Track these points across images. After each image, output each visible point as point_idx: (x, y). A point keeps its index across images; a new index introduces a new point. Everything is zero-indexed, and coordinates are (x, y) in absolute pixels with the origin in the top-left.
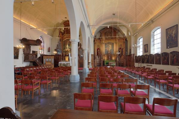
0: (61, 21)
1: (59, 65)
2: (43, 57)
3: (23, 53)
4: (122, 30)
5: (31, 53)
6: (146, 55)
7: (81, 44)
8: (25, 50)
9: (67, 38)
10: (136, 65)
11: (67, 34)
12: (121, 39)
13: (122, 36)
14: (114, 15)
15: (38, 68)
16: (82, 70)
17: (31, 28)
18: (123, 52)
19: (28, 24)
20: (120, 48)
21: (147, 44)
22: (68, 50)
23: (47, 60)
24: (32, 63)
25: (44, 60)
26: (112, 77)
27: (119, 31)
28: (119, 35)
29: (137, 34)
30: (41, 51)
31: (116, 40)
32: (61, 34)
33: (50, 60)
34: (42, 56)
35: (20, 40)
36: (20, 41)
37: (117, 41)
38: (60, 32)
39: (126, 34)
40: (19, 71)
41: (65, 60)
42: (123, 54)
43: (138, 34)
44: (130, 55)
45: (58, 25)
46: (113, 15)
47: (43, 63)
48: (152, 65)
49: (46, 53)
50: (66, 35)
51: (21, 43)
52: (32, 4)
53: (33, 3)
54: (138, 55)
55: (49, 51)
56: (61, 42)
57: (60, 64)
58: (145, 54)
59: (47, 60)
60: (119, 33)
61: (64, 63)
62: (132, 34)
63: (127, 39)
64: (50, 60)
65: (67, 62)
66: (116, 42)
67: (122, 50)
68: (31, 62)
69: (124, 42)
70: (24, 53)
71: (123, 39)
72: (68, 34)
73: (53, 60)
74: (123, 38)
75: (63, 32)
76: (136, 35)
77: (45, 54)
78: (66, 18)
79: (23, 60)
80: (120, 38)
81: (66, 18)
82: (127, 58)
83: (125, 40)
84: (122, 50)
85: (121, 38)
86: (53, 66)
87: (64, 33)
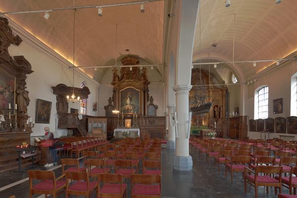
0: (116, 56)
1: (114, 135)
2: (87, 120)
3: (56, 112)
4: (219, 73)
5: (69, 112)
6: (279, 118)
7: (151, 97)
8: (60, 108)
9: (130, 86)
10: (253, 135)
11: (128, 79)
12: (218, 90)
13: (218, 85)
14: (215, 46)
15: (80, 142)
16: (166, 143)
17: (70, 67)
18: (221, 113)
19: (66, 58)
20: (217, 106)
21: (281, 99)
22: (130, 108)
23: (95, 125)
24: (72, 131)
25: (90, 125)
26: (29, 126)
27: (214, 77)
28: (214, 83)
29: (255, 81)
30: (82, 108)
31: (209, 91)
32: (117, 79)
33: (100, 125)
34: (86, 118)
35: (53, 88)
36: (53, 90)
37: (211, 93)
38: (115, 76)
39: (226, 82)
40: (61, 147)
41: (124, 126)
42: (221, 116)
43: (257, 81)
44: (238, 119)
45: (112, 62)
46: (213, 47)
47: (87, 129)
48: (294, 137)
49: (90, 113)
50: (127, 80)
51: (54, 93)
52: (99, 13)
53: (100, 11)
54: (256, 118)
55: (95, 110)
56: (150, 96)
57: (117, 133)
58: (275, 116)
59: (95, 125)
60: (214, 80)
61: (123, 130)
62: (243, 81)
63: (229, 91)
64: (100, 125)
65: (129, 130)
66: (209, 94)
67: (220, 109)
68: (69, 129)
69: (223, 96)
70: (58, 113)
71: (222, 91)
72: (129, 80)
73: (105, 125)
74: (220, 87)
75: (120, 75)
76: (252, 82)
77: (89, 115)
78: (127, 50)
79: (57, 125)
80: (216, 88)
81: (127, 50)
82: (228, 123)
83: (224, 92)
84: (220, 109)
85: (218, 88)
86: (105, 136)
87: (122, 78)
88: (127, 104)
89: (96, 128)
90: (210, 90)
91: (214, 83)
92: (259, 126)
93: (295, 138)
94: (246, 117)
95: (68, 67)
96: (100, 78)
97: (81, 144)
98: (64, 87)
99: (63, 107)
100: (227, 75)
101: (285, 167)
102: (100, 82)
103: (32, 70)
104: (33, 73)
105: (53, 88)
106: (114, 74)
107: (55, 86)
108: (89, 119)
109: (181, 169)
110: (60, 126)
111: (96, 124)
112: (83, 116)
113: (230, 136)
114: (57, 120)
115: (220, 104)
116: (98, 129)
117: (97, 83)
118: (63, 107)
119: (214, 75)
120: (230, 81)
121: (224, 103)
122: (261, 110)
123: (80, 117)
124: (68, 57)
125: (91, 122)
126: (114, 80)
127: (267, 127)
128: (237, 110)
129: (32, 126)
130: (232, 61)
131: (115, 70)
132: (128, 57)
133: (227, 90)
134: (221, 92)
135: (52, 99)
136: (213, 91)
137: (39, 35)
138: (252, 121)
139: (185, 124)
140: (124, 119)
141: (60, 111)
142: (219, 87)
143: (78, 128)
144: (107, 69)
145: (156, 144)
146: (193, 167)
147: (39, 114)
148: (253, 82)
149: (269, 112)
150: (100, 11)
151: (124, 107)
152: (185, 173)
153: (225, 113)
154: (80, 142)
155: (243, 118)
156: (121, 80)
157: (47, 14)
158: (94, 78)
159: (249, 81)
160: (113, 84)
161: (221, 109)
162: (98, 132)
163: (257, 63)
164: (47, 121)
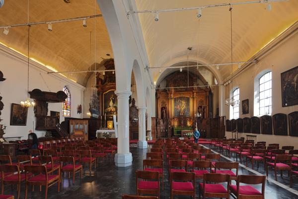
2: (69, 121)
4: (202, 75)
5: (49, 114)
6: (246, 119)
7: (133, 99)
10: (229, 135)
11: (111, 82)
13: (202, 86)
16: (136, 143)
17: (48, 73)
18: (205, 114)
21: (248, 100)
22: (112, 110)
25: (71, 127)
28: (198, 85)
30: (63, 110)
31: (193, 93)
32: (100, 82)
33: (81, 127)
34: (68, 120)
35: (29, 93)
37: (195, 94)
38: (98, 79)
39: (210, 83)
41: (107, 127)
42: (205, 117)
48: (256, 136)
50: (110, 84)
51: (31, 98)
53: (50, 27)
54: (231, 118)
57: (99, 134)
58: (243, 117)
60: (199, 82)
62: (221, 82)
63: (212, 92)
64: (81, 127)
66: (193, 96)
71: (206, 92)
73: (86, 127)
75: (103, 78)
76: (227, 83)
78: (108, 55)
80: (200, 89)
81: (108, 55)
83: (208, 93)
84: (204, 109)
85: (202, 89)
88: (110, 107)
91: (198, 85)
92: (234, 125)
93: (257, 137)
94: (223, 117)
95: (47, 73)
97: (49, 145)
99: (42, 110)
102: (85, 85)
103: (4, 77)
107: (31, 91)
109: (119, 165)
110: (38, 128)
111: (78, 125)
114: (35, 122)
117: (82, 87)
118: (42, 110)
119: (199, 77)
121: (207, 104)
125: (72, 124)
126: (97, 83)
131: (98, 74)
133: (210, 91)
135: (30, 103)
136: (197, 93)
138: (228, 121)
141: (38, 114)
142: (202, 88)
144: (92, 73)
145: (229, 153)
147: (13, 117)
148: (229, 84)
151: (107, 109)
152: (123, 169)
153: (209, 114)
158: (77, 83)
159: (226, 82)
160: (97, 87)
164: (23, 122)
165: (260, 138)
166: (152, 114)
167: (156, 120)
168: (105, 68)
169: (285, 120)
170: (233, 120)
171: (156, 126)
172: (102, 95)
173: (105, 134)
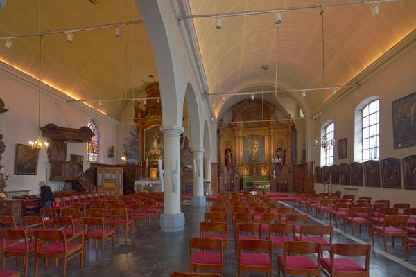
1: (135, 189)
2: (96, 169)
3: (47, 159)
5: (68, 159)
6: (343, 165)
7: (186, 138)
10: (319, 188)
13: (282, 120)
14: (266, 69)
16: (190, 199)
17: (68, 101)
18: (286, 158)
20: (280, 149)
21: (346, 139)
24: (71, 184)
25: (100, 176)
28: (276, 118)
31: (270, 129)
32: (140, 115)
33: (113, 176)
34: (95, 167)
35: (41, 129)
37: (272, 130)
38: (137, 110)
39: (292, 116)
42: (286, 163)
44: (304, 165)
48: (357, 190)
50: (153, 116)
53: (70, 37)
57: (138, 186)
59: (108, 176)
60: (278, 113)
63: (296, 127)
64: (113, 176)
65: (153, 182)
66: (270, 133)
67: (284, 152)
70: (50, 161)
71: (288, 128)
73: (120, 177)
75: (144, 109)
76: (317, 116)
77: (103, 163)
78: (151, 76)
79: (48, 177)
80: (279, 124)
81: (151, 76)
83: (290, 129)
84: (284, 152)
85: (283, 125)
89: (109, 180)
90: (270, 127)
94: (312, 163)
96: (118, 114)
98: (54, 128)
99: (58, 153)
100: (293, 106)
101: (265, 225)
104: (8, 112)
105: (41, 129)
106: (135, 108)
107: (44, 126)
108: (99, 169)
111: (108, 175)
112: (92, 164)
113: (295, 189)
115: (285, 146)
116: (111, 183)
120: (298, 115)
122: (327, 158)
123: (86, 167)
124: (64, 90)
125: (101, 172)
126: (136, 116)
127: (333, 178)
128: (304, 158)
129: (5, 178)
130: (274, 93)
131: (138, 103)
132: (153, 85)
133: (293, 128)
134: (286, 130)
137: (17, 65)
138: (318, 168)
139: (172, 175)
140: (149, 168)
143: (82, 180)
146: (185, 225)
149: (334, 156)
150: (70, 37)
152: (172, 234)
154: (83, 197)
155: (309, 165)
156: (145, 116)
157: (8, 42)
158: (108, 115)
160: (136, 121)
161: (287, 152)
162: (112, 185)
163: (306, 92)
165: (362, 192)
166: (213, 158)
167: (219, 167)
168: (147, 95)
169: (397, 167)
170: (325, 167)
171: (219, 176)
172: (142, 132)
173: (147, 187)
